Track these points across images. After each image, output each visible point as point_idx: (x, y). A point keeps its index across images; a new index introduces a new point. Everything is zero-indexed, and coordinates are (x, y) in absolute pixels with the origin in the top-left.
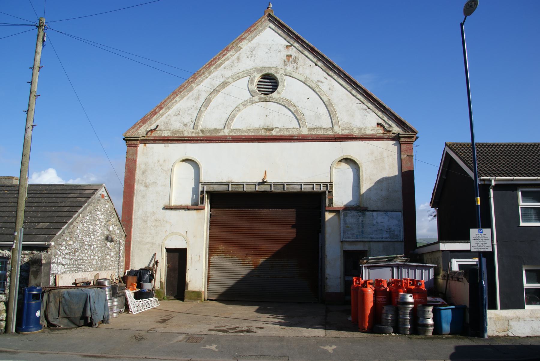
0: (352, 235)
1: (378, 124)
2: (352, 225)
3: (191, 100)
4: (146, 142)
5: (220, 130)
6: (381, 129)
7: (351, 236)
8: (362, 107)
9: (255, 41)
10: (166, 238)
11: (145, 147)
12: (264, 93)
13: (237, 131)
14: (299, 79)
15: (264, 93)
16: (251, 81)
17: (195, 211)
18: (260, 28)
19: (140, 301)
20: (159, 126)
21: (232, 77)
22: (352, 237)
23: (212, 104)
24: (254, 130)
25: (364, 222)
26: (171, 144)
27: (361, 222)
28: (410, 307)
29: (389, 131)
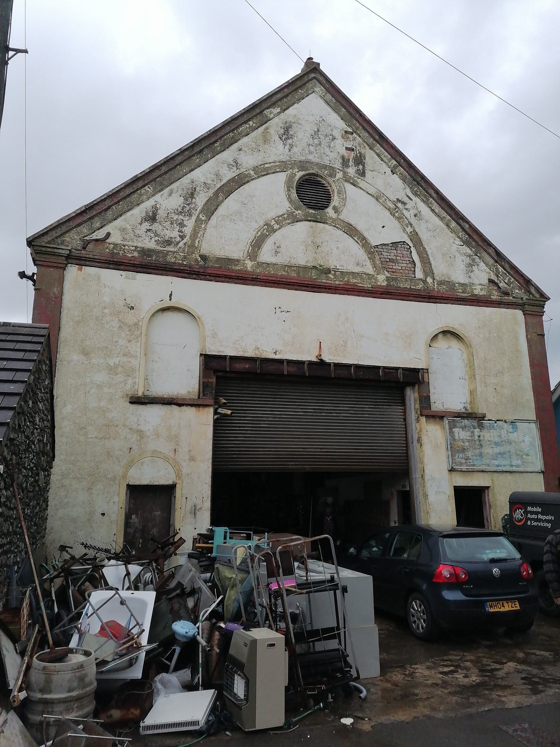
0: (466, 459)
1: (491, 281)
2: (463, 442)
3: (406, 209)
4: (83, 262)
5: (238, 261)
6: (495, 290)
7: (463, 461)
8: (465, 251)
9: (291, 111)
10: (130, 464)
11: (79, 272)
12: (308, 205)
13: (269, 267)
14: (361, 191)
15: (308, 205)
16: (290, 179)
17: (193, 408)
18: (300, 91)
19: (17, 736)
20: (111, 235)
21: (255, 169)
22: (466, 463)
23: (221, 210)
24: (299, 268)
25: (482, 438)
26: (138, 274)
27: (477, 438)
28: (218, 146)
29: (507, 294)
